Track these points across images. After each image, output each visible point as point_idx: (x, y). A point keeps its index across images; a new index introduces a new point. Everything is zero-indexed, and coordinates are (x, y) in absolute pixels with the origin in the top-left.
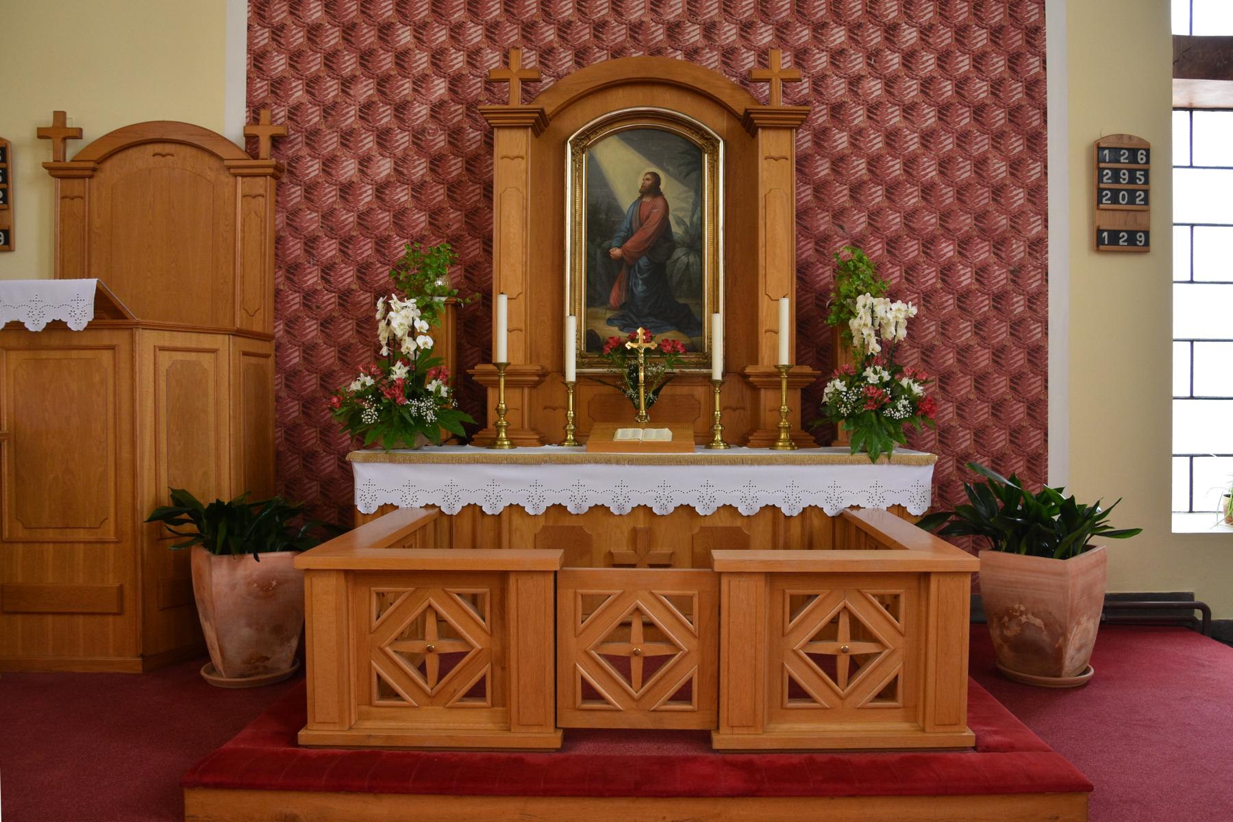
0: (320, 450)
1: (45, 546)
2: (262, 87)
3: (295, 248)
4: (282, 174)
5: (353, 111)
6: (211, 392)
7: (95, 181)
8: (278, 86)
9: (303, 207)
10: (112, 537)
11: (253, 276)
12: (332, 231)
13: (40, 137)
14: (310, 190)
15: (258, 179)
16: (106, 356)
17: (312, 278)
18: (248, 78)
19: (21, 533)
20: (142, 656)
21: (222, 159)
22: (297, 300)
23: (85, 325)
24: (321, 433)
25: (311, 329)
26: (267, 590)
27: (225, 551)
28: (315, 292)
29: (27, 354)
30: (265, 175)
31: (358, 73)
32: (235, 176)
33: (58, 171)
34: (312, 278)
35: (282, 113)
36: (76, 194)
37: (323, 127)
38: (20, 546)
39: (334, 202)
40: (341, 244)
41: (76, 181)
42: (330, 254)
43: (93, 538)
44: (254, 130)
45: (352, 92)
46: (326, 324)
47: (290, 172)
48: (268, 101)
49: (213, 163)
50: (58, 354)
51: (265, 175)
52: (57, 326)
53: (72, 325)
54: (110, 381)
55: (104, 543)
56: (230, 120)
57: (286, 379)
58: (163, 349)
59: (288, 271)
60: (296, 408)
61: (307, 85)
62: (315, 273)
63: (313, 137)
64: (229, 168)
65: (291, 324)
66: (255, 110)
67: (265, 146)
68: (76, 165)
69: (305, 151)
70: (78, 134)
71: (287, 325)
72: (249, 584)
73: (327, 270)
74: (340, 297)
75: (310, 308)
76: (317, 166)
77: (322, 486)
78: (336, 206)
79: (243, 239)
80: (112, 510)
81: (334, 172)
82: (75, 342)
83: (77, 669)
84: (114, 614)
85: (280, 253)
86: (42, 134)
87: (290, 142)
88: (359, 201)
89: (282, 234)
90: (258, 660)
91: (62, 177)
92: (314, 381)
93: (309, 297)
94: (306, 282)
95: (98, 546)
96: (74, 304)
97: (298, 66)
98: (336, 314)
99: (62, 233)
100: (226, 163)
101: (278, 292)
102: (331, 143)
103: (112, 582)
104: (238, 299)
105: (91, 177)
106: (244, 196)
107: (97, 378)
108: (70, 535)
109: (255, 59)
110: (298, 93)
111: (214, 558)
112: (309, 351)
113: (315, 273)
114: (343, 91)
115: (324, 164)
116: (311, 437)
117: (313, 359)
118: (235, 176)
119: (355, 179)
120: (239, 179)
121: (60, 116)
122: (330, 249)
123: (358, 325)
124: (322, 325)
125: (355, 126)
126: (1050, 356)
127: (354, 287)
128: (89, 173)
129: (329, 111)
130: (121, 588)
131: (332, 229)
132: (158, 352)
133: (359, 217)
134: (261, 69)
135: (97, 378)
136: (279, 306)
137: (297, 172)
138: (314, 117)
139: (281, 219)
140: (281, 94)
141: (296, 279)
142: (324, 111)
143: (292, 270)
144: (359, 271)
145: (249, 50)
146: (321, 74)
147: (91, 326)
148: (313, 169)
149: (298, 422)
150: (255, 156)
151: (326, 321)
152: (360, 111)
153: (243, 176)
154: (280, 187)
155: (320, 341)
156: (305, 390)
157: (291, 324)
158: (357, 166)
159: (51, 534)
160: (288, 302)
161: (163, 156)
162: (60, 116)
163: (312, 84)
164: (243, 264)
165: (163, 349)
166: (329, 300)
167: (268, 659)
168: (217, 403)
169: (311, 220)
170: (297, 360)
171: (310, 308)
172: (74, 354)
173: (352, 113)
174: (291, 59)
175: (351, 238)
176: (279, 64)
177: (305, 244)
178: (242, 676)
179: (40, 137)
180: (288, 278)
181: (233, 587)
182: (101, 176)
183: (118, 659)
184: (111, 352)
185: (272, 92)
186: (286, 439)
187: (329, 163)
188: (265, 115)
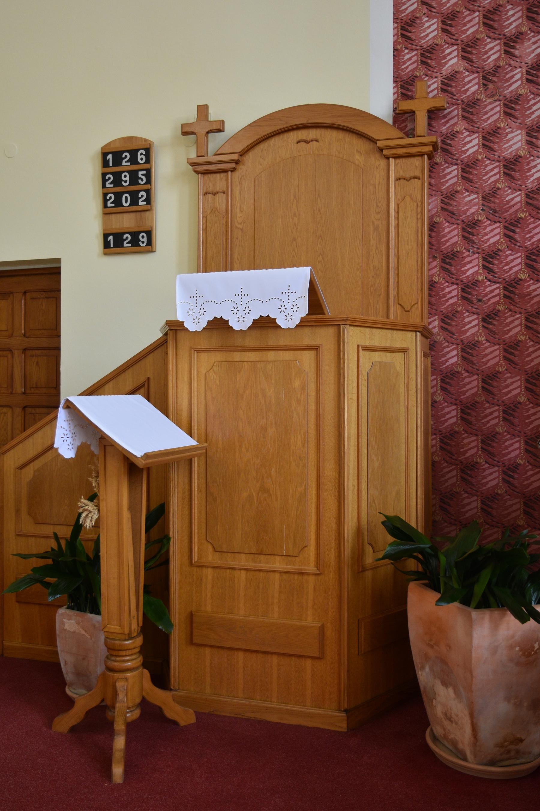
0: (481, 461)
1: (237, 573)
2: (411, 58)
3: (452, 235)
4: (441, 150)
5: (518, 74)
6: (402, 398)
7: (237, 175)
8: (429, 56)
9: (460, 188)
10: (311, 567)
11: (411, 264)
12: (494, 215)
13: (184, 133)
14: (468, 169)
15: (412, 160)
16: (308, 357)
17: (472, 268)
18: (395, 50)
19: (211, 557)
20: (346, 711)
21: (373, 141)
22: (455, 293)
23: (298, 321)
24: (483, 442)
25: (471, 325)
26: (529, 655)
27: (484, 604)
28: (476, 283)
29: (219, 357)
30: (421, 155)
31: (524, 29)
32: (387, 158)
33: (202, 169)
34: (472, 268)
35: (434, 85)
36: (218, 189)
37: (482, 97)
38: (210, 570)
39: (497, 181)
40: (505, 227)
41: (218, 176)
42: (492, 241)
43: (289, 568)
44: (406, 105)
45: (517, 52)
46: (489, 318)
47: (444, 150)
48: (418, 74)
49: (363, 145)
50: (252, 356)
51: (421, 155)
52: (266, 324)
53: (235, 325)
54: (312, 386)
55: (302, 574)
56: (378, 100)
57: (442, 381)
58: (366, 349)
59: (443, 261)
60: (454, 413)
61: (464, 50)
62: (476, 262)
63: (471, 109)
64: (381, 150)
65: (448, 319)
66: (404, 86)
67: (422, 120)
68: (218, 158)
69: (461, 126)
70: (219, 128)
71: (442, 321)
72: (511, 647)
73: (490, 258)
74: (505, 289)
75: (470, 301)
76: (476, 142)
77: (483, 502)
78: (499, 185)
79: (397, 226)
80: (313, 537)
81: (496, 147)
82: (239, 342)
83: (274, 718)
84: (314, 658)
85: (433, 241)
86: (186, 131)
87: (444, 117)
88: (527, 178)
89: (436, 220)
90: (512, 743)
91: (204, 173)
92: (475, 383)
93: (468, 289)
94: (464, 272)
95: (296, 577)
96: (285, 297)
97: (453, 30)
98: (500, 308)
99: (205, 230)
100: (379, 144)
101: (432, 285)
102: (492, 113)
103: (311, 620)
104: (392, 292)
105: (233, 170)
106: (397, 179)
107: (297, 384)
108: (265, 563)
109: (403, 28)
110: (452, 60)
111: (475, 614)
112: (469, 349)
113: (476, 262)
114: (506, 52)
115: (484, 138)
116: (471, 447)
117: (474, 359)
118: (387, 158)
119: (521, 153)
120: (392, 161)
121: (203, 110)
122: (492, 235)
123: (527, 319)
124: (484, 320)
125: (522, 92)
126: (61, 358)
127: (522, 276)
128: (232, 165)
129: (490, 77)
130: (322, 629)
131: (495, 211)
132: (362, 353)
133: (527, 196)
134: (409, 38)
135: (297, 384)
136: (433, 299)
137: (453, 150)
138: (472, 86)
139: (433, 204)
140: (433, 63)
141: (453, 269)
142: (484, 78)
143: (448, 260)
144: (528, 257)
145: (396, 19)
146: (480, 36)
147: (304, 323)
148: (472, 145)
149: (456, 428)
150: (411, 134)
151: (488, 316)
152: (528, 73)
153: (396, 157)
154: (433, 166)
155: (482, 339)
156: (464, 393)
157: (448, 319)
158: (525, 137)
159: (243, 561)
160: (444, 296)
161: (306, 142)
162: (203, 110)
163: (468, 50)
164: (397, 255)
165: (366, 349)
166: (493, 292)
167: (521, 741)
168: (407, 408)
169: (470, 203)
170: (455, 360)
171: (470, 301)
172: (271, 355)
173: (518, 76)
174: (443, 22)
175: (519, 220)
176: (430, 30)
177: (464, 229)
178: (492, 763)
179: (184, 133)
180: (443, 269)
181: (494, 650)
182: (242, 170)
183: (316, 711)
184: (313, 353)
185: (423, 62)
186: (441, 448)
187: (491, 138)
188: (419, 88)
